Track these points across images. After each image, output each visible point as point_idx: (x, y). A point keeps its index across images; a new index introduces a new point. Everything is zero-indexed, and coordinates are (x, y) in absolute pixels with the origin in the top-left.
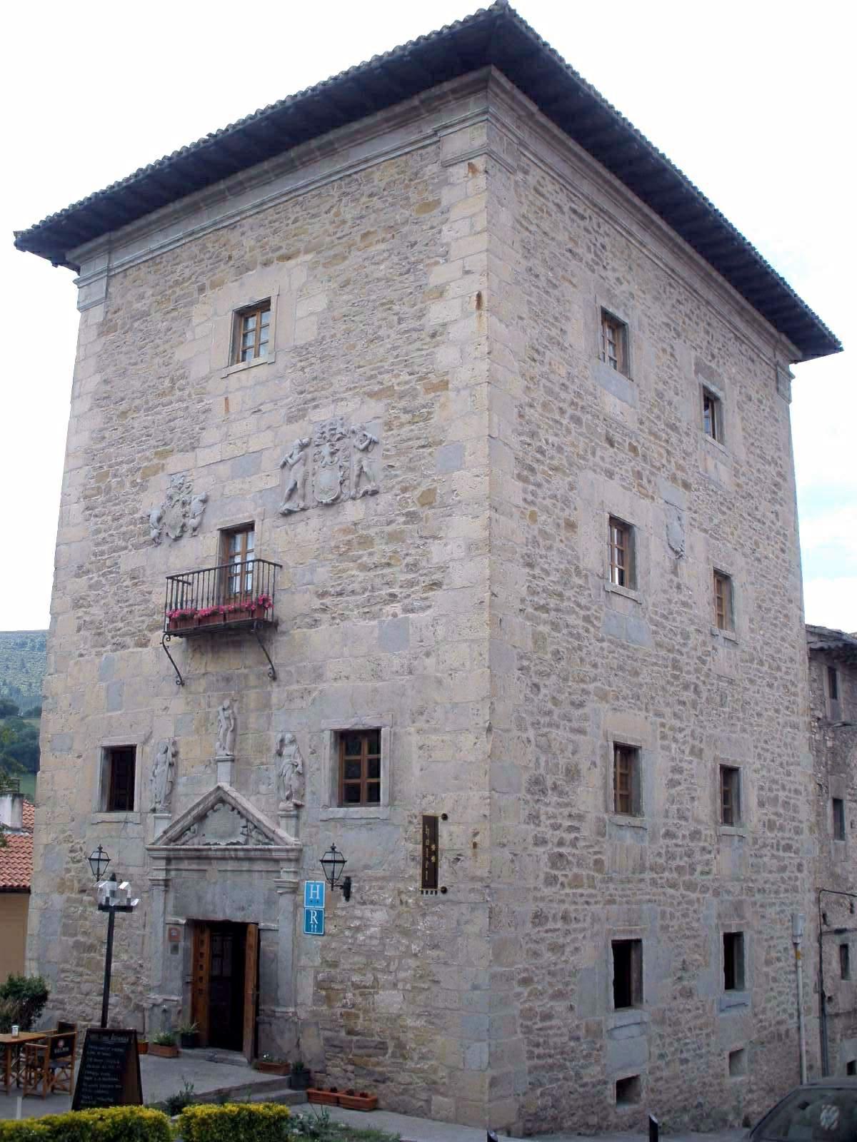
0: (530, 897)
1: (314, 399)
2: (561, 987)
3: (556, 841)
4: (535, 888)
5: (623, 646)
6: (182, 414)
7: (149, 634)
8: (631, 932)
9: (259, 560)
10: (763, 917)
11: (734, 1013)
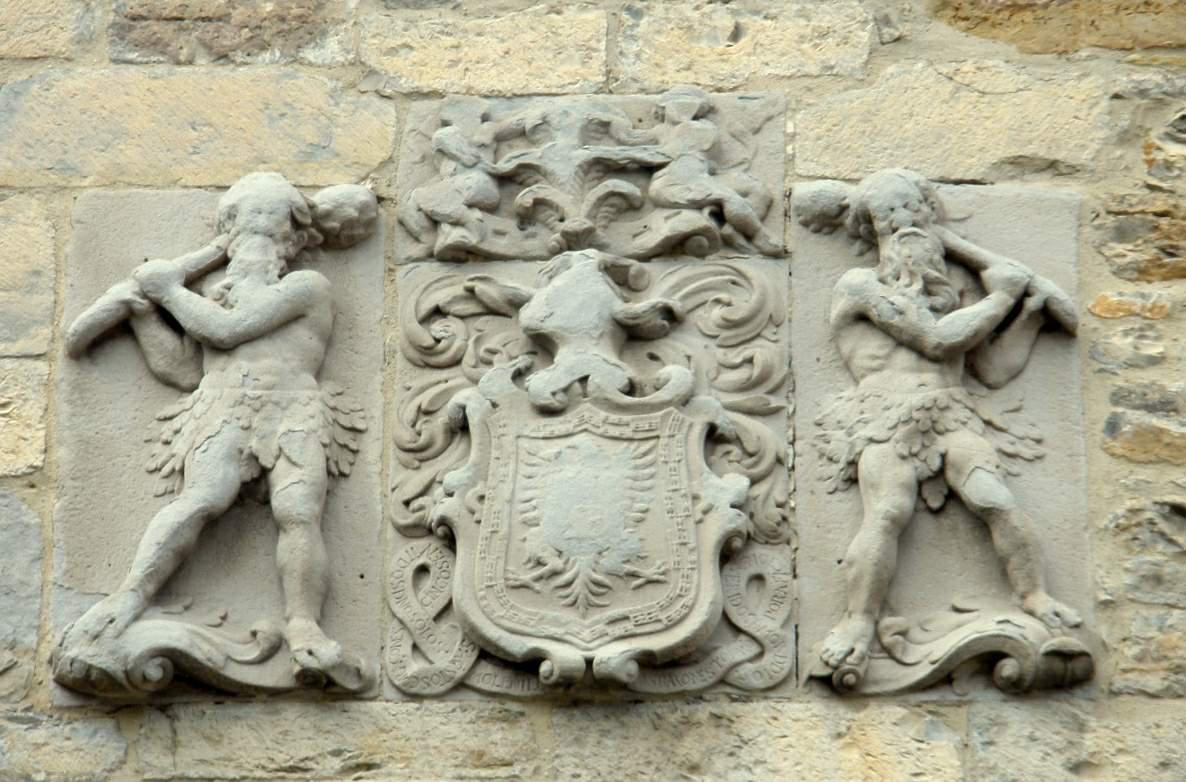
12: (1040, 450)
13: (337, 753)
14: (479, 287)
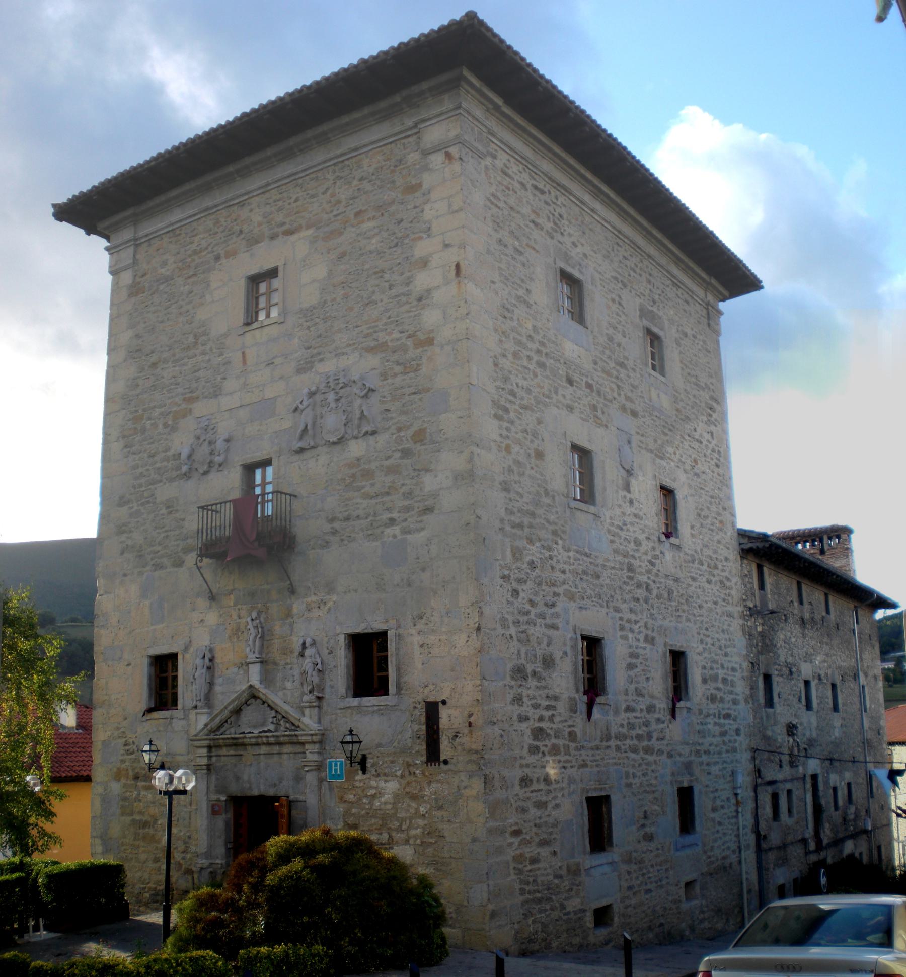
0: (517, 764)
1: (319, 354)
2: (545, 836)
3: (536, 717)
4: (521, 757)
5: (586, 555)
6: (205, 365)
8: (601, 789)
9: (277, 492)
10: (709, 773)
11: (688, 851)
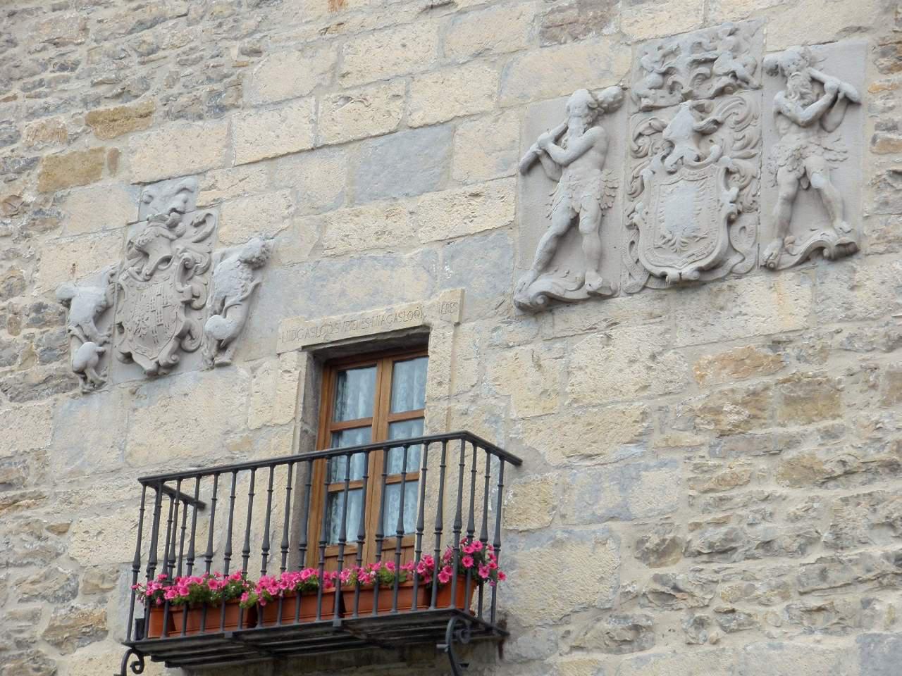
7: (54, 656)
12: (846, 155)
13: (605, 320)
14: (653, 122)
